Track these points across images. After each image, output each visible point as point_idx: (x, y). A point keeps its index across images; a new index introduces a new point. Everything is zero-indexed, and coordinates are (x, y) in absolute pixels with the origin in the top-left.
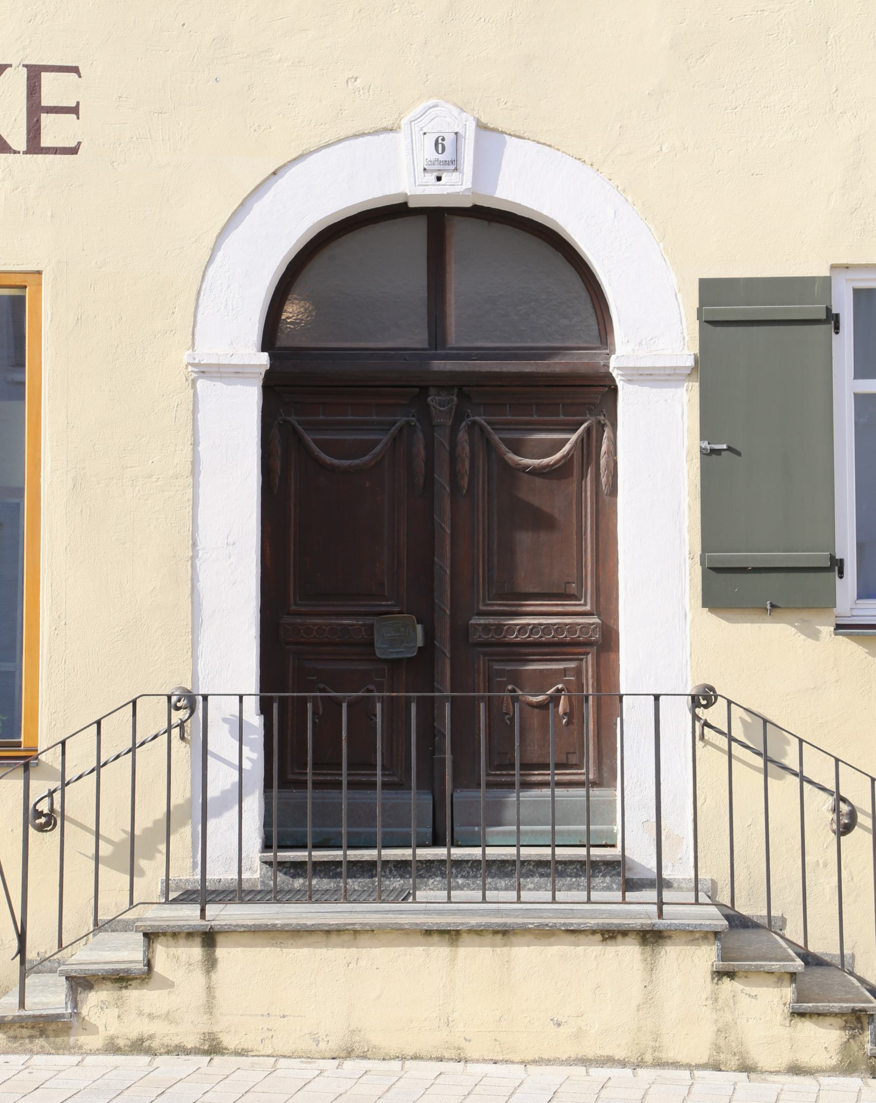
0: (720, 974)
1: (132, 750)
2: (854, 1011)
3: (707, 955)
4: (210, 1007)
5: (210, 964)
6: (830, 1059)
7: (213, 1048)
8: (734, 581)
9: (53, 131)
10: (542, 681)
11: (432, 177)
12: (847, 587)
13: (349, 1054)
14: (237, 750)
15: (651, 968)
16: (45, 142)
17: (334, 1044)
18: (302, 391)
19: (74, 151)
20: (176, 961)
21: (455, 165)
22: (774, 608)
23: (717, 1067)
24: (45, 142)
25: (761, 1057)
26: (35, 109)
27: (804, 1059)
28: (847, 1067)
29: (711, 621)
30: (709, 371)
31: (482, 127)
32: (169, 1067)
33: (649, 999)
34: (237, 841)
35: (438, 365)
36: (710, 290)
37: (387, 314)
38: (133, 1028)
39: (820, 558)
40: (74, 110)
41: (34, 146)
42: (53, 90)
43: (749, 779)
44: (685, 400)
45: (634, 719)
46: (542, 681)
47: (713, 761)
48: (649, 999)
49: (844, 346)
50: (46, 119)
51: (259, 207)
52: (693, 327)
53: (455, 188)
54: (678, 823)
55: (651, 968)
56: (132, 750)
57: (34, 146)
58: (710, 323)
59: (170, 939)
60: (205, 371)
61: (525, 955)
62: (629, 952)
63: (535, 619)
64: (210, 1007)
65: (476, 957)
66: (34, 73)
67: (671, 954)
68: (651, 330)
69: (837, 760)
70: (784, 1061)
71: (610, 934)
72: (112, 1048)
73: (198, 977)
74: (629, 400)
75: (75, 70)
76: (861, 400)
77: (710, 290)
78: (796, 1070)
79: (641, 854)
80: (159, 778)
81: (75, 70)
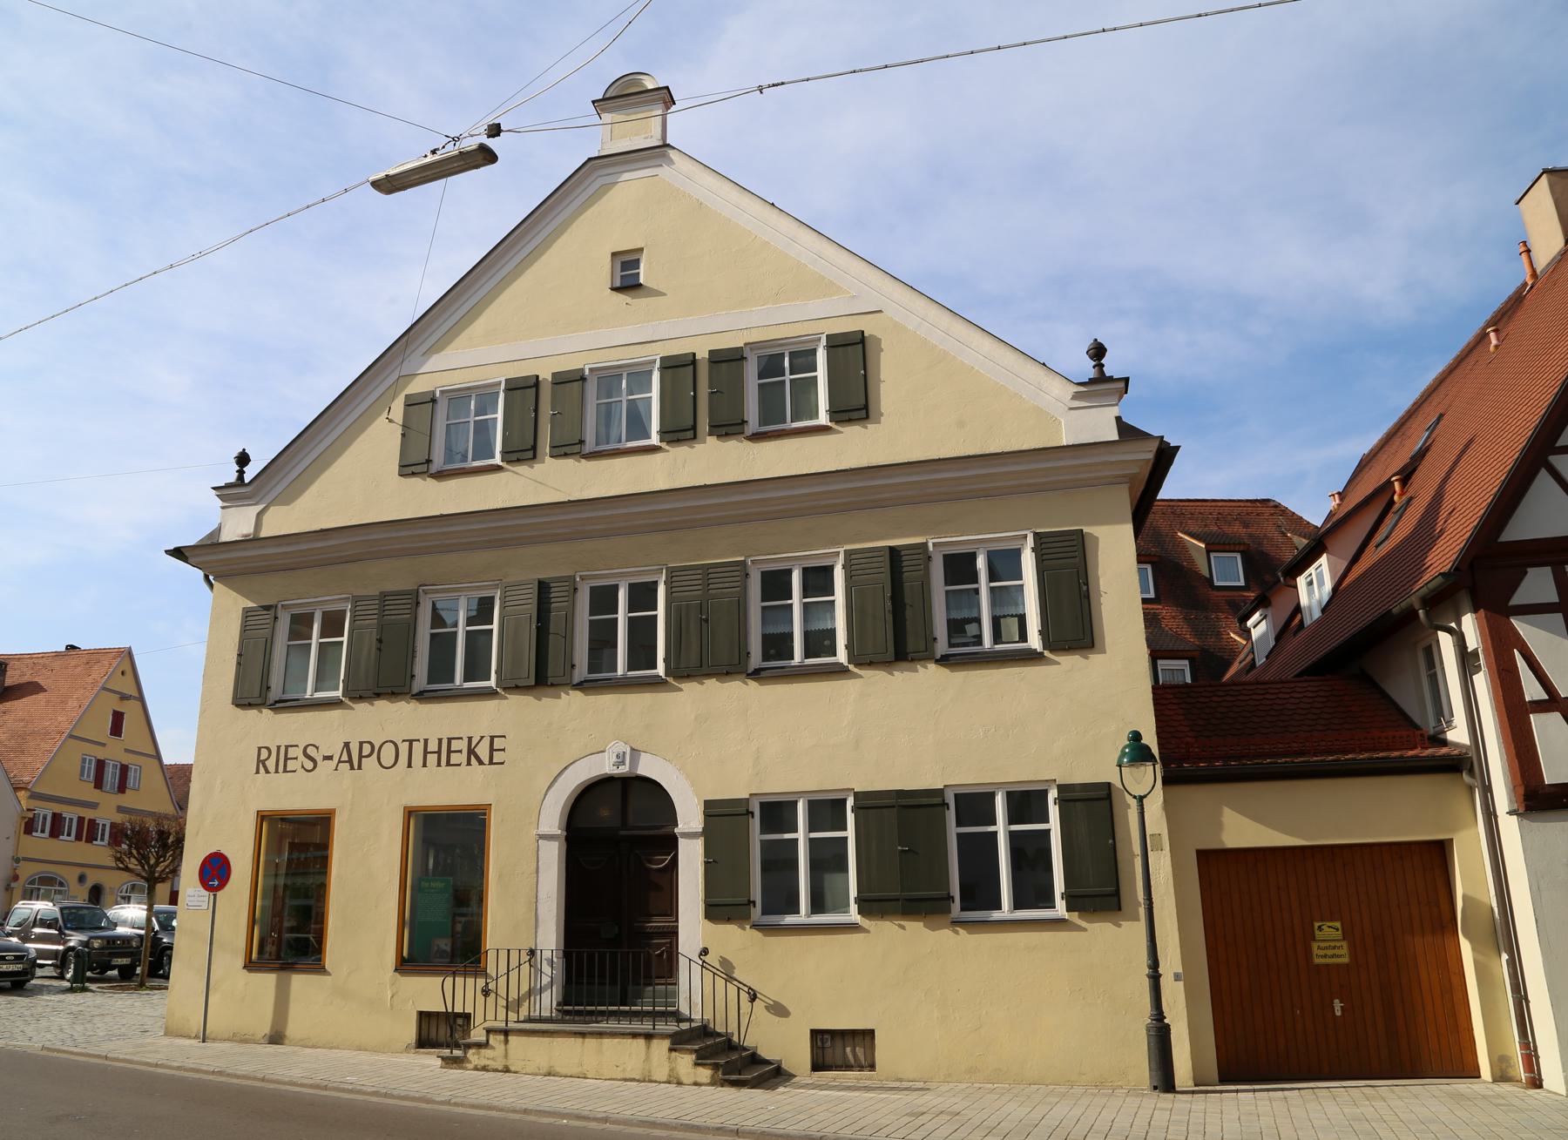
0: (671, 1050)
3: (666, 1043)
4: (506, 1056)
5: (506, 1042)
6: (707, 1080)
7: (507, 1070)
8: (716, 910)
9: (497, 757)
10: (659, 946)
12: (756, 912)
13: (549, 1074)
14: (550, 971)
15: (648, 1047)
17: (544, 1071)
20: (496, 1040)
21: (623, 763)
22: (729, 920)
23: (669, 1082)
25: (684, 1079)
26: (492, 750)
27: (699, 1080)
28: (713, 1083)
30: (708, 833)
31: (632, 749)
32: (491, 1074)
33: (647, 1059)
34: (548, 1002)
35: (623, 833)
36: (708, 804)
37: (606, 814)
38: (484, 1062)
39: (745, 900)
41: (491, 763)
42: (498, 743)
43: (720, 982)
44: (699, 844)
45: (683, 963)
46: (659, 946)
47: (708, 975)
48: (647, 1059)
49: (756, 823)
51: (560, 780)
52: (701, 818)
53: (624, 770)
54: (697, 998)
55: (648, 1047)
57: (491, 763)
58: (708, 816)
60: (542, 837)
61: (607, 1042)
62: (641, 1042)
63: (657, 923)
64: (506, 1056)
65: (591, 1042)
66: (492, 738)
67: (655, 1042)
68: (689, 818)
70: (691, 1081)
71: (635, 1035)
72: (476, 1069)
73: (502, 1046)
74: (682, 843)
76: (959, 835)
77: (708, 804)
78: (696, 1084)
79: (684, 1009)
80: (522, 980)
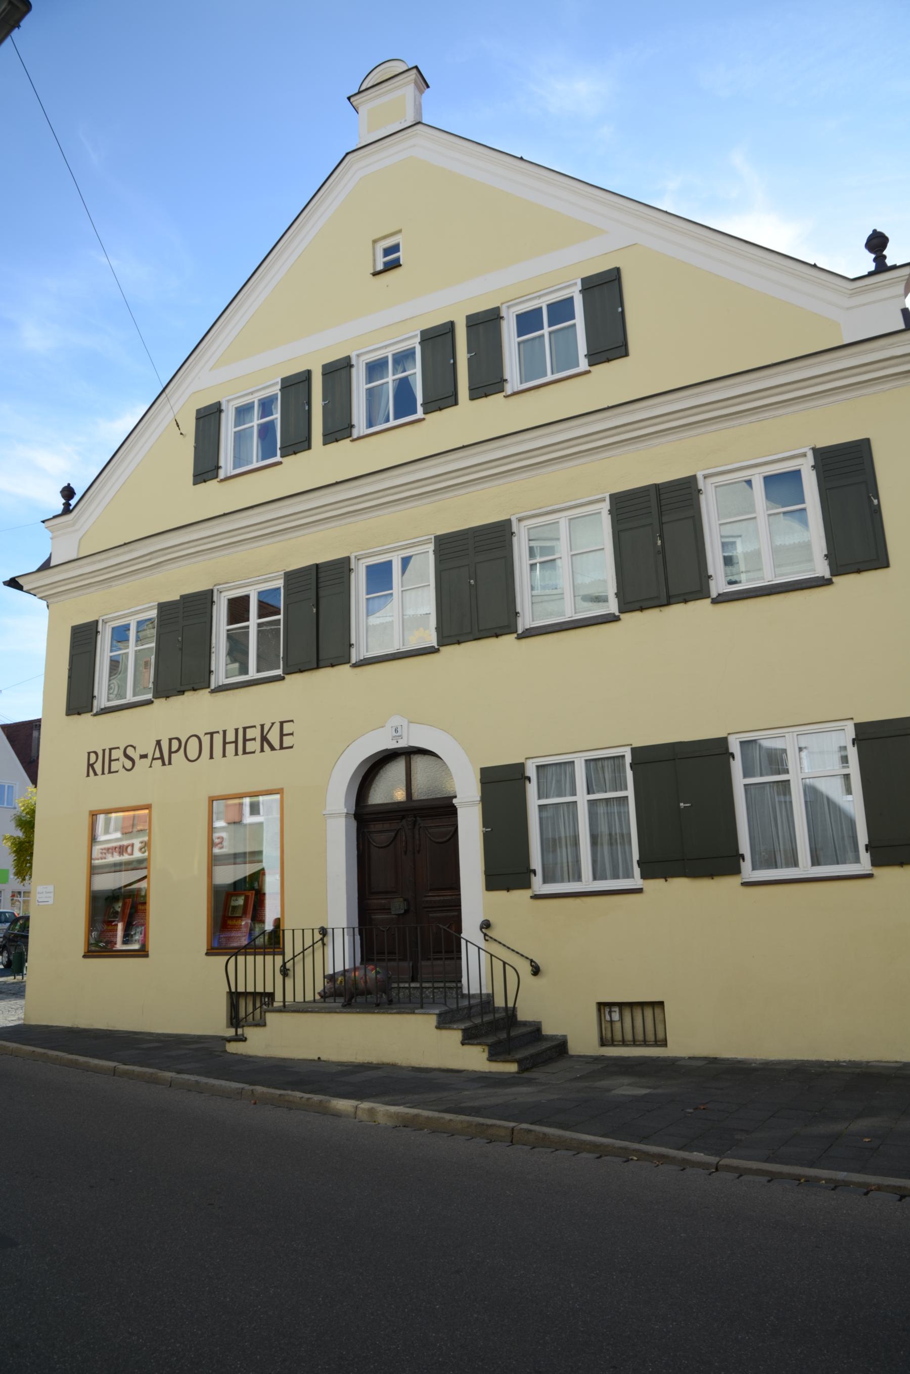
1: (314, 944)
2: (120, 847)
11: (395, 741)
16: (285, 745)
18: (366, 818)
19: (291, 747)
21: (401, 737)
24: (285, 745)
29: (438, 1032)
36: (484, 771)
40: (292, 734)
42: (287, 728)
50: (285, 738)
56: (314, 944)
59: (387, 1006)
66: (282, 723)
69: (504, 963)
75: (292, 721)
77: (484, 771)
81: (292, 721)
